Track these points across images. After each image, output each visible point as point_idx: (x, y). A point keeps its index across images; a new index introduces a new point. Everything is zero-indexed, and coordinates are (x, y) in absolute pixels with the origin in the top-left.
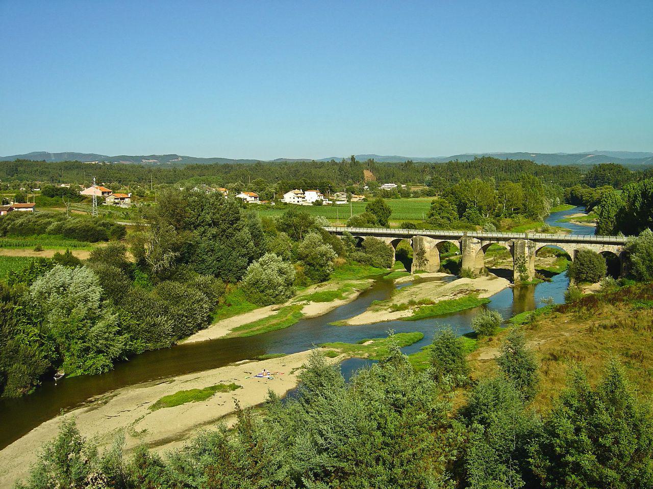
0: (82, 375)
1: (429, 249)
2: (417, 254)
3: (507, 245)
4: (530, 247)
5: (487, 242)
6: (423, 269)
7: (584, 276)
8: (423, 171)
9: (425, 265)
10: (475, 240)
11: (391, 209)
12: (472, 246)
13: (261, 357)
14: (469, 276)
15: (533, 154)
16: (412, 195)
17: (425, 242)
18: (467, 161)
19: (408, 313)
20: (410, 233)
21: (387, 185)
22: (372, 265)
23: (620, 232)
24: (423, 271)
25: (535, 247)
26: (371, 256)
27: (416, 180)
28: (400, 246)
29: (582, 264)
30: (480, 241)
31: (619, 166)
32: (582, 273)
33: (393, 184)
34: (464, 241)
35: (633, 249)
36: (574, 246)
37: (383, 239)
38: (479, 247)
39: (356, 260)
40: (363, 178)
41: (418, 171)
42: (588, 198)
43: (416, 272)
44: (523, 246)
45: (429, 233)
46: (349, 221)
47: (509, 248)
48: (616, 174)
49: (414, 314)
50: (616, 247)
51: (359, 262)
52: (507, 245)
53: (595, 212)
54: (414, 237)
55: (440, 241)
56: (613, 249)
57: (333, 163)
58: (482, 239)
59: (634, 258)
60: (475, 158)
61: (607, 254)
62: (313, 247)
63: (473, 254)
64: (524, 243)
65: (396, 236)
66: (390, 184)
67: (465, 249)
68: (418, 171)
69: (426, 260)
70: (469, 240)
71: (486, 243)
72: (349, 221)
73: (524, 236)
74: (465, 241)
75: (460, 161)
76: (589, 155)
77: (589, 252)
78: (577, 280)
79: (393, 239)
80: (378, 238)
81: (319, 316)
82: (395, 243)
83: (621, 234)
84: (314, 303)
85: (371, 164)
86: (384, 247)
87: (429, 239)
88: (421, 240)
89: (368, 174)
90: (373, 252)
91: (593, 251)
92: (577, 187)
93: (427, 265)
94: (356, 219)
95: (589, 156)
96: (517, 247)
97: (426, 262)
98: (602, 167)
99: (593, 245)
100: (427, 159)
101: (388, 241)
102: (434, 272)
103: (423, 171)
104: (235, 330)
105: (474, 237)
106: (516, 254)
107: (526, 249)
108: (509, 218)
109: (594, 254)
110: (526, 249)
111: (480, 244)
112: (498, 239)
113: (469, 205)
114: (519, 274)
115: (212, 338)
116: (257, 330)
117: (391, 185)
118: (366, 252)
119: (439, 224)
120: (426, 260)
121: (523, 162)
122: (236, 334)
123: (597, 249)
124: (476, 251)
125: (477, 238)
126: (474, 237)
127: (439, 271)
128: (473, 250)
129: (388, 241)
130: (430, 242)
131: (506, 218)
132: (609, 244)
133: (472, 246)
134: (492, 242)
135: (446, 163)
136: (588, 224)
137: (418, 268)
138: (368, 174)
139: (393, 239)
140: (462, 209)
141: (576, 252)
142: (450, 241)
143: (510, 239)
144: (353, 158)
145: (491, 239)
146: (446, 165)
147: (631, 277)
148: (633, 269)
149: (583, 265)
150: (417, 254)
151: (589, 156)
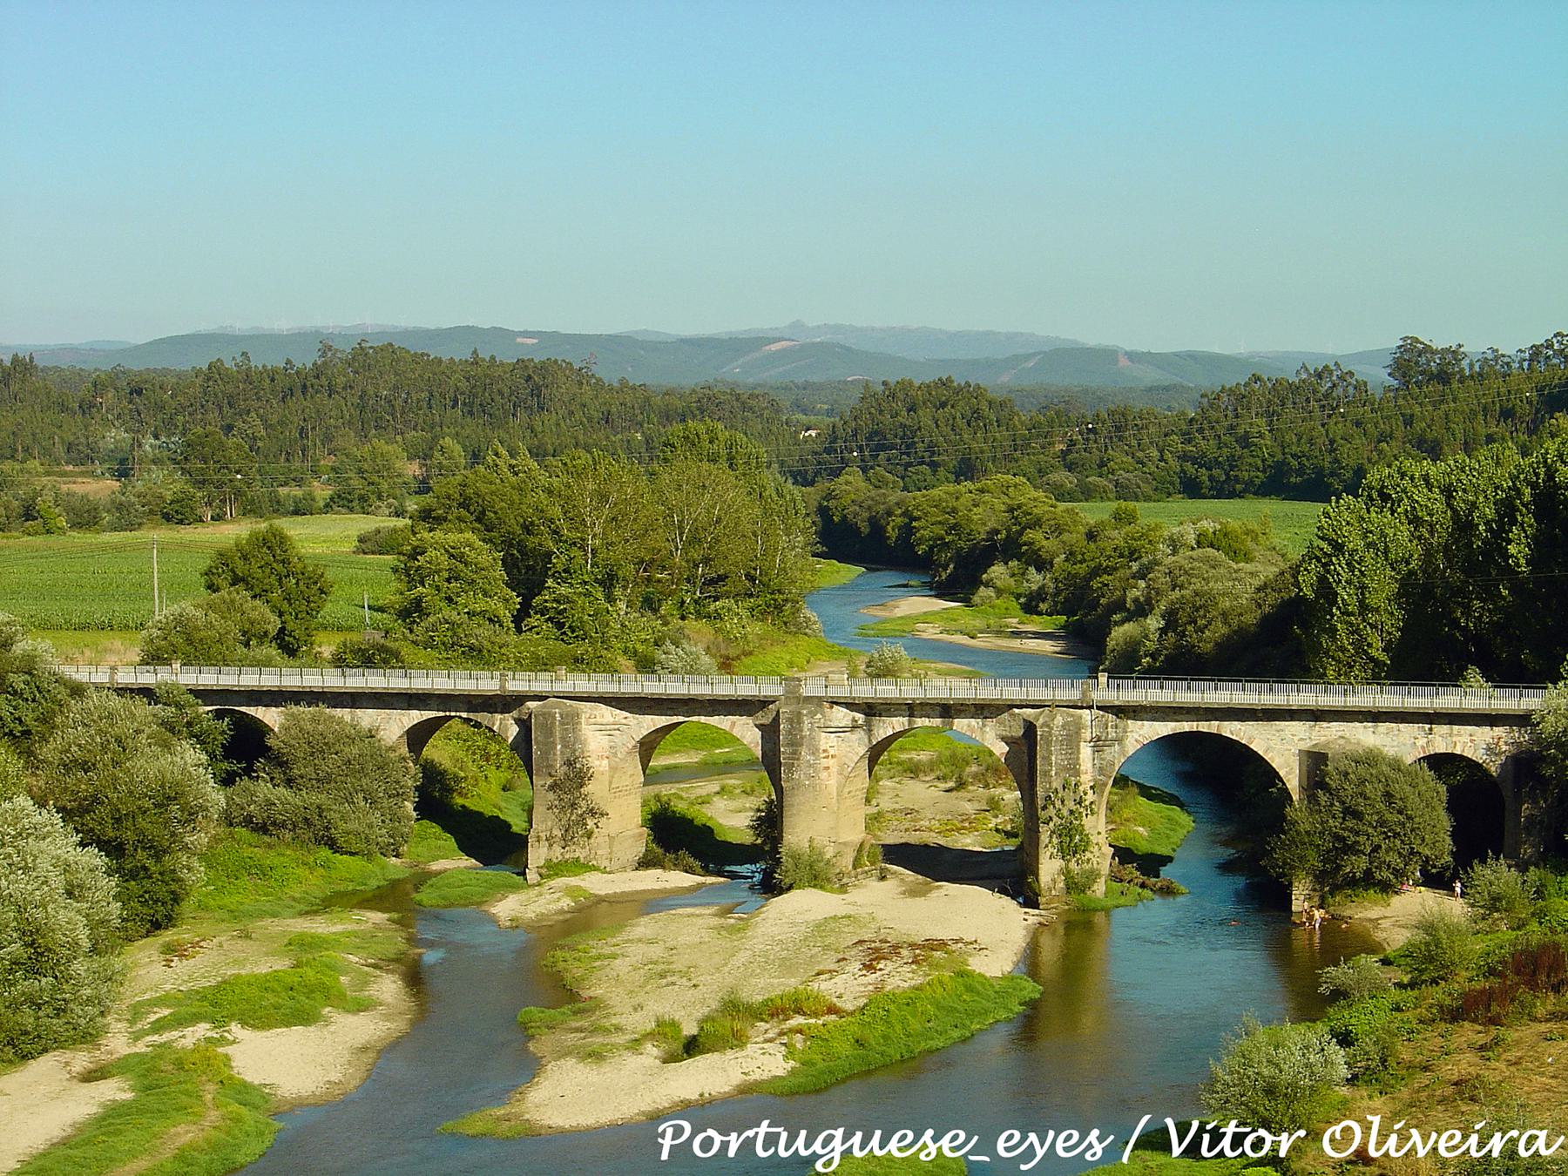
1: (605, 762)
2: (552, 788)
3: (992, 738)
4: (1098, 744)
5: (898, 723)
6: (580, 853)
7: (1362, 863)
8: (87, 407)
9: (589, 835)
10: (842, 716)
11: (329, 575)
12: (826, 741)
16: (107, 518)
18: (288, 362)
22: (333, 845)
24: (580, 867)
25: (1120, 740)
26: (316, 798)
27: (60, 450)
28: (439, 751)
29: (1351, 812)
30: (860, 717)
32: (1352, 849)
34: (790, 721)
36: (1300, 735)
37: (367, 717)
38: (857, 746)
39: (248, 821)
41: (64, 408)
43: (552, 869)
44: (1072, 739)
45: (607, 686)
46: (156, 633)
47: (1001, 749)
48: (961, 423)
49: (792, 1063)
50: (1485, 734)
51: (263, 829)
52: (746, 731)
54: (532, 705)
55: (663, 721)
56: (1471, 743)
58: (872, 710)
60: (326, 349)
61: (1441, 763)
62: (116, 764)
67: (795, 755)
68: (64, 408)
69: (592, 812)
70: (812, 714)
72: (156, 633)
74: (796, 719)
75: (257, 362)
77: (1370, 759)
78: (1322, 884)
79: (416, 716)
80: (344, 714)
81: (1157, 1149)
82: (418, 737)
83: (1474, 674)
84: (259, 1036)
86: (377, 760)
87: (607, 713)
88: (572, 720)
90: (328, 779)
92: (848, 483)
93: (599, 838)
94: (181, 624)
95: (775, 347)
96: (1049, 743)
97: (590, 823)
99: (1383, 727)
101: (394, 725)
102: (624, 869)
103: (87, 407)
106: (1046, 773)
107: (1086, 751)
108: (699, 616)
109: (1396, 765)
110: (1086, 751)
113: (558, 562)
114: (1058, 863)
118: (289, 782)
119: (472, 648)
120: (592, 812)
121: (544, 368)
124: (842, 766)
125: (851, 705)
126: (834, 702)
127: (645, 863)
128: (831, 762)
129: (394, 725)
130: (608, 730)
131: (683, 618)
133: (826, 741)
134: (920, 722)
135: (198, 373)
136: (1016, 644)
137: (557, 850)
139: (416, 716)
141: (1315, 761)
145: (911, 709)
146: (199, 381)
149: (1358, 815)
150: (552, 788)
151: (775, 347)
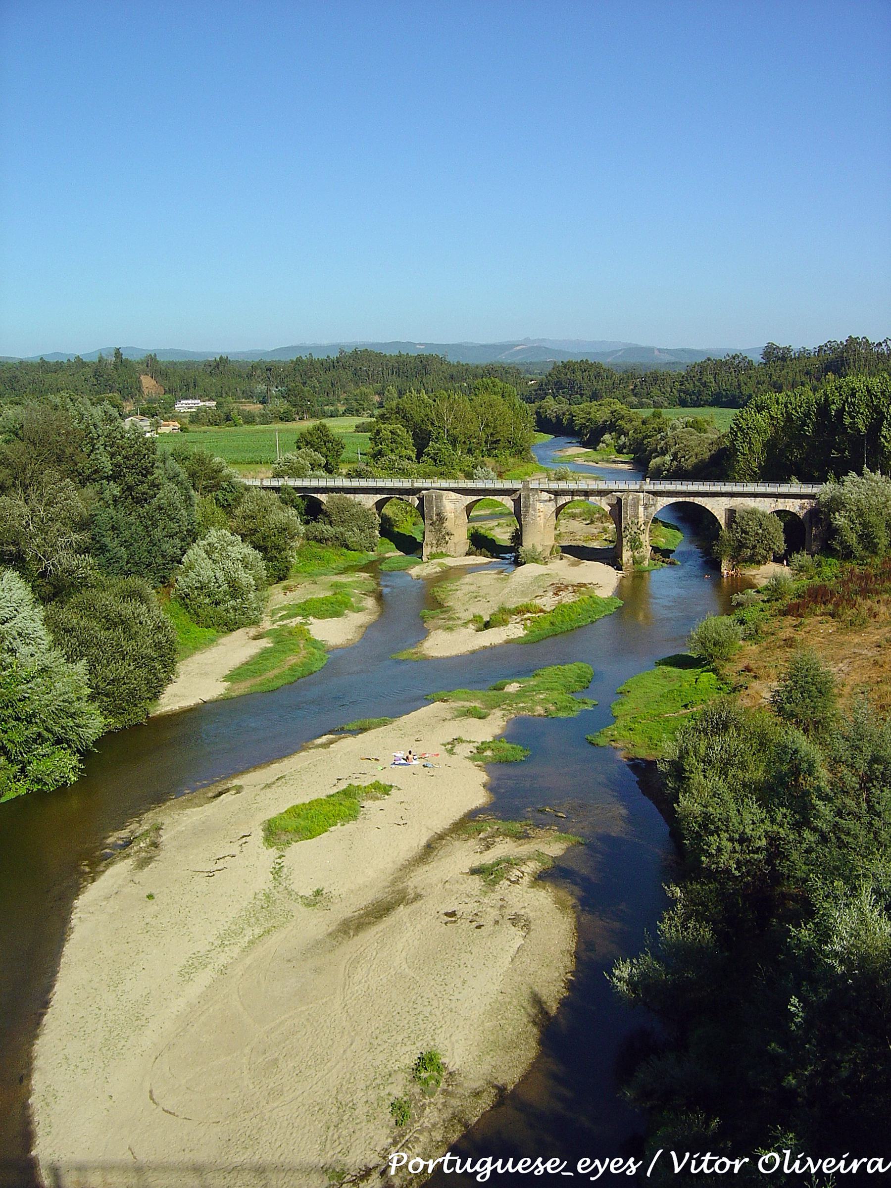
0: (30, 793)
3: (604, 504)
4: (646, 507)
5: (568, 498)
8: (250, 376)
10: (545, 496)
13: (350, 727)
14: (535, 560)
15: (421, 344)
17: (446, 502)
18: (328, 357)
19: (515, 630)
20: (416, 485)
21: (186, 402)
22: (347, 547)
23: (793, 477)
25: (654, 505)
27: (240, 393)
28: (387, 510)
31: (597, 366)
33: (196, 401)
34: (525, 498)
35: (835, 504)
37: (360, 497)
38: (551, 507)
40: (140, 390)
42: (583, 421)
43: (432, 556)
44: (636, 505)
45: (453, 484)
53: (607, 445)
54: (424, 492)
56: (793, 506)
57: (80, 363)
58: (557, 493)
59: (840, 520)
63: (541, 521)
64: (638, 499)
65: (386, 492)
66: (190, 402)
67: (527, 511)
70: (534, 495)
71: (563, 500)
73: (637, 487)
75: (315, 357)
76: (518, 345)
77: (753, 512)
79: (379, 497)
82: (380, 505)
85: (152, 365)
87: (453, 495)
88: (439, 498)
89: (147, 382)
91: (761, 509)
95: (518, 348)
97: (447, 538)
98: (568, 366)
99: (758, 499)
100: (373, 345)
101: (369, 501)
104: (234, 676)
105: (542, 491)
106: (626, 518)
107: (641, 509)
110: (641, 509)
111: (553, 503)
112: (587, 493)
114: (630, 553)
115: (206, 698)
116: (276, 677)
117: (193, 402)
122: (242, 688)
123: (766, 506)
124: (545, 515)
125: (549, 492)
126: (542, 491)
127: (468, 554)
128: (541, 514)
129: (369, 501)
132: (785, 498)
133: (539, 506)
134: (576, 498)
137: (434, 548)
138: (147, 382)
140: (421, 440)
141: (731, 513)
142: (495, 498)
143: (419, 490)
144: (118, 353)
145: (573, 493)
147: (828, 551)
148: (835, 539)
149: (747, 533)
151: (518, 348)
